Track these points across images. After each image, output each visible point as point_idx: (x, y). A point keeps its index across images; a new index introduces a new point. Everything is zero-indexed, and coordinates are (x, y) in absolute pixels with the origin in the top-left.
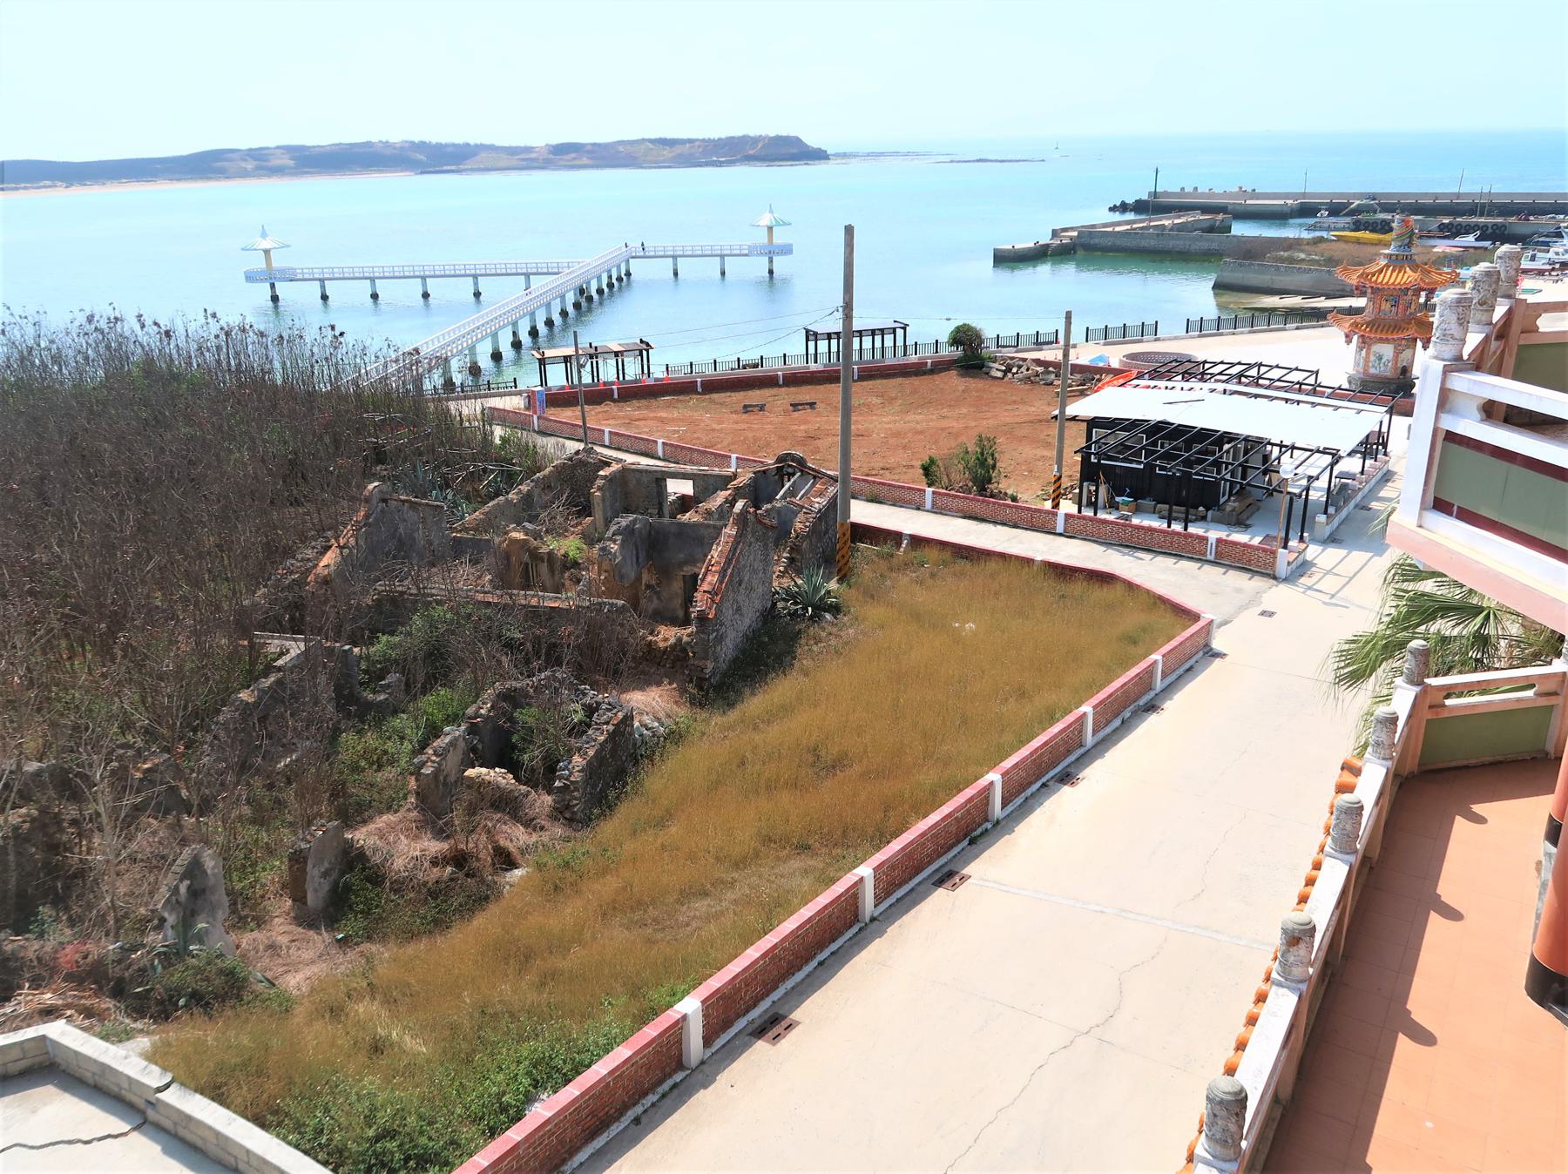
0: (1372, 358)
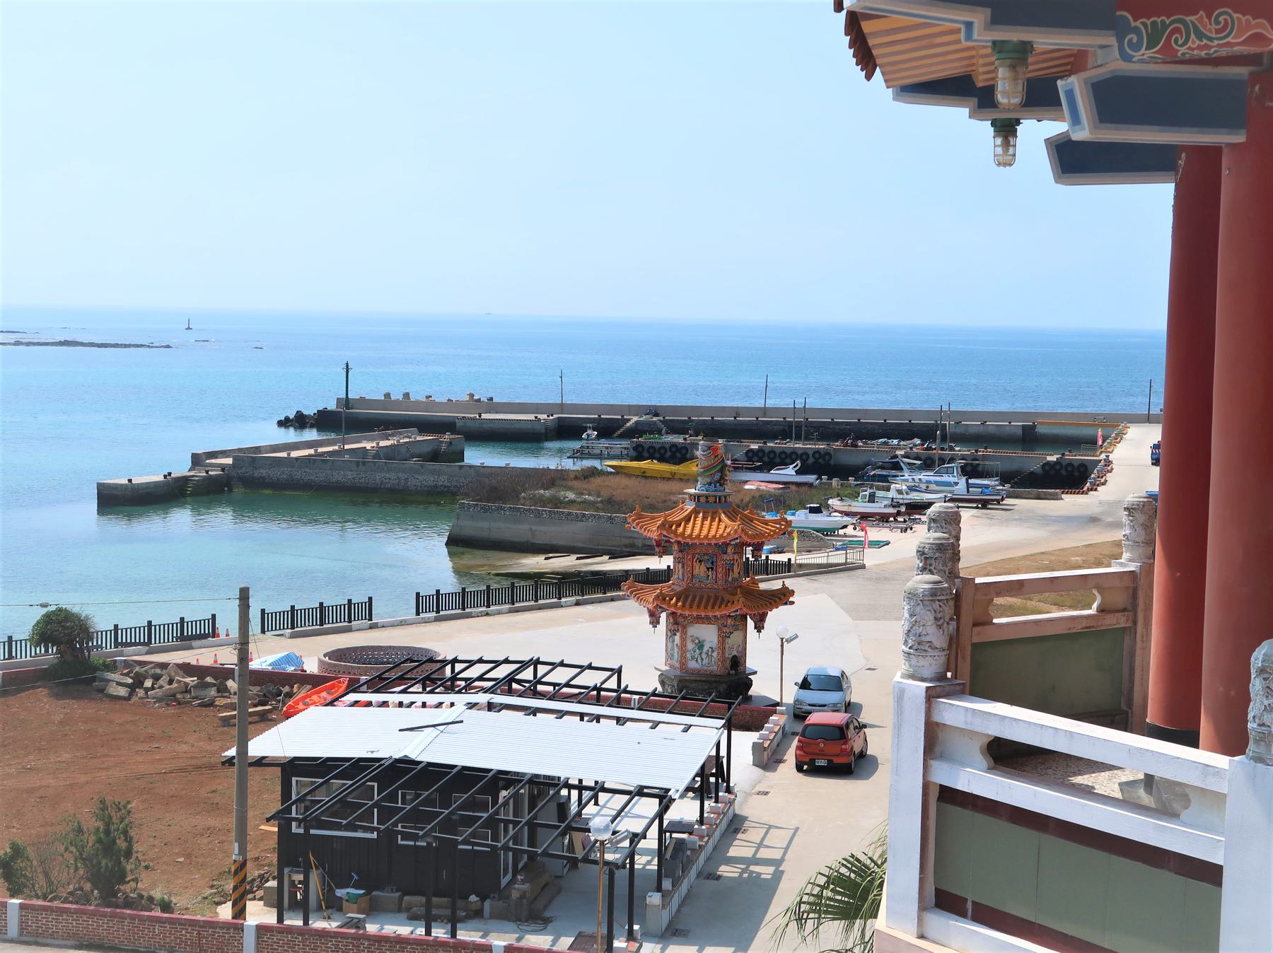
0: (690, 646)
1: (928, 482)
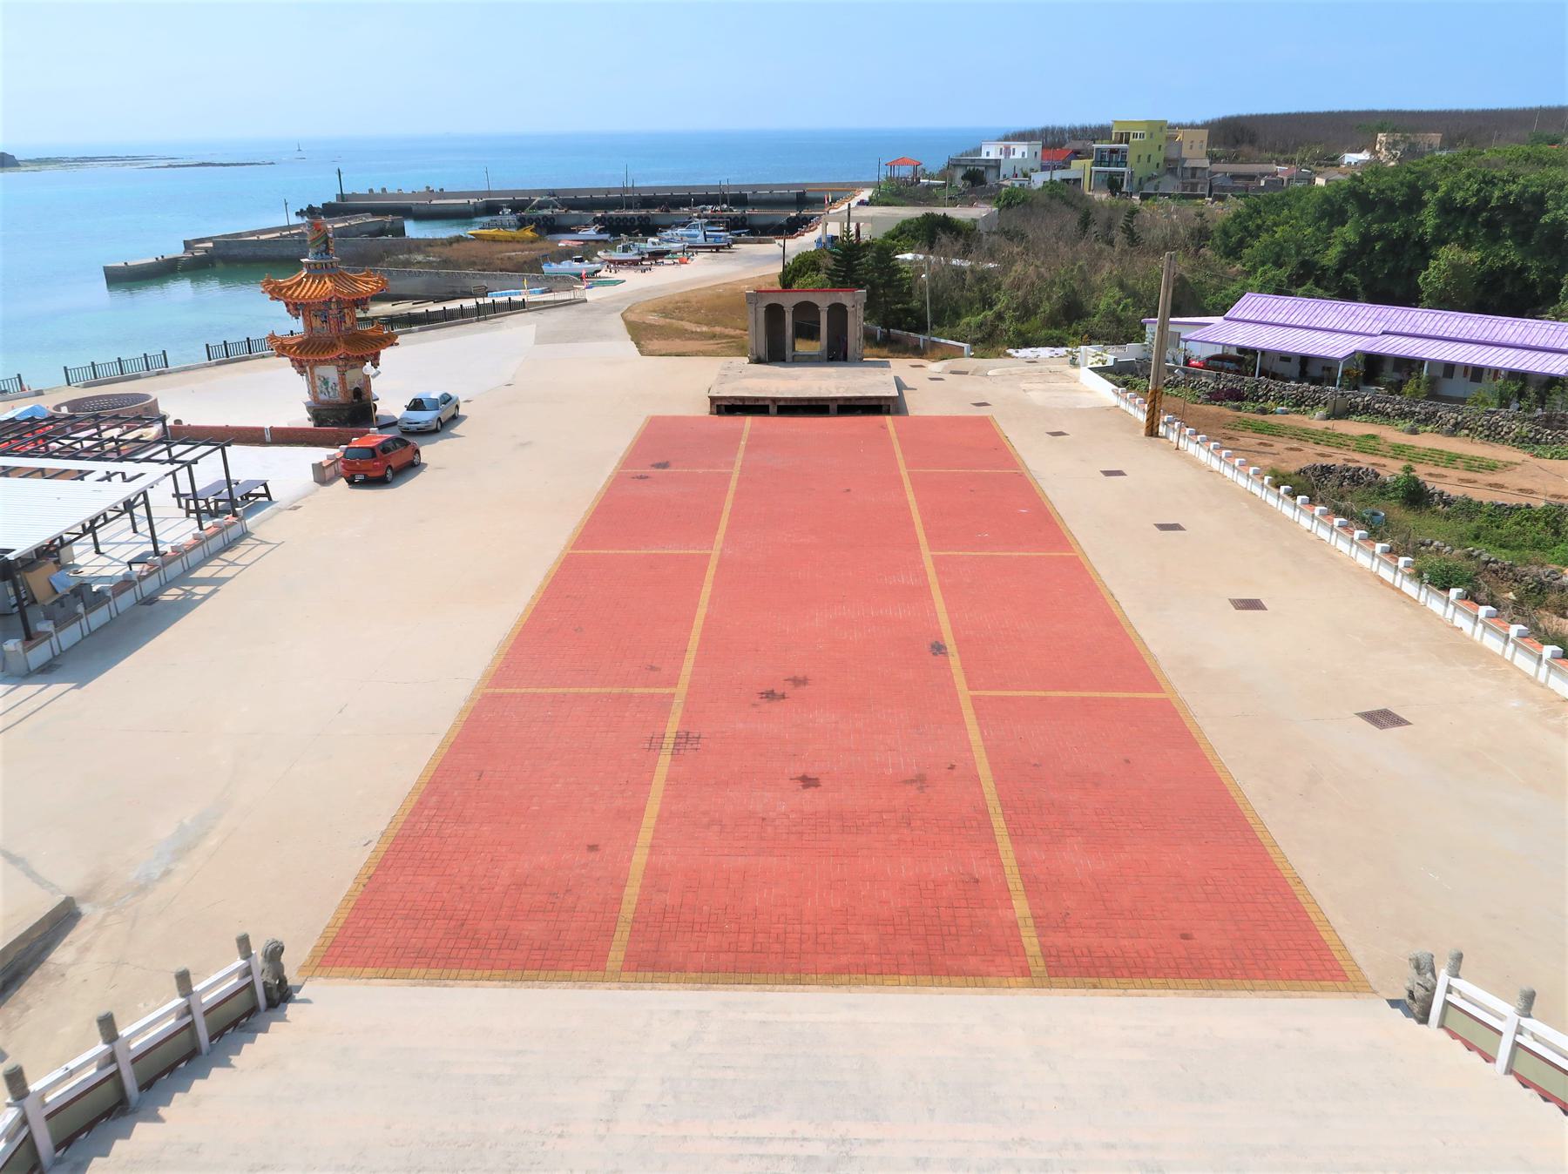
0: (318, 383)
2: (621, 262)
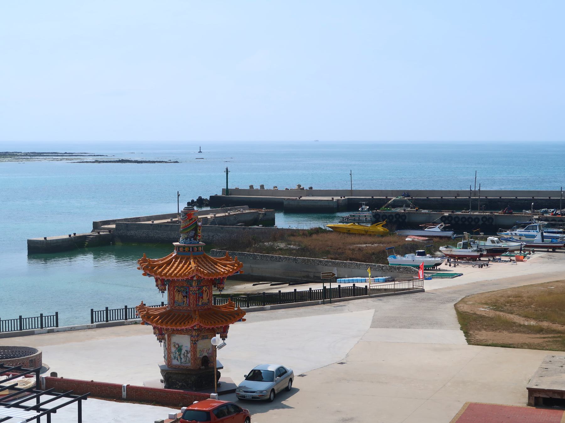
0: (173, 349)
1: (521, 235)
2: (461, 257)
